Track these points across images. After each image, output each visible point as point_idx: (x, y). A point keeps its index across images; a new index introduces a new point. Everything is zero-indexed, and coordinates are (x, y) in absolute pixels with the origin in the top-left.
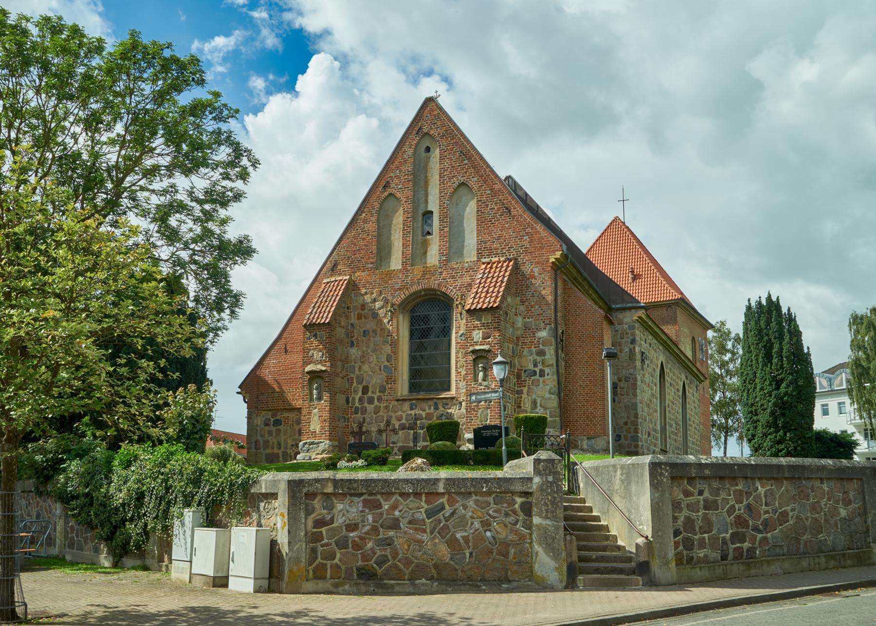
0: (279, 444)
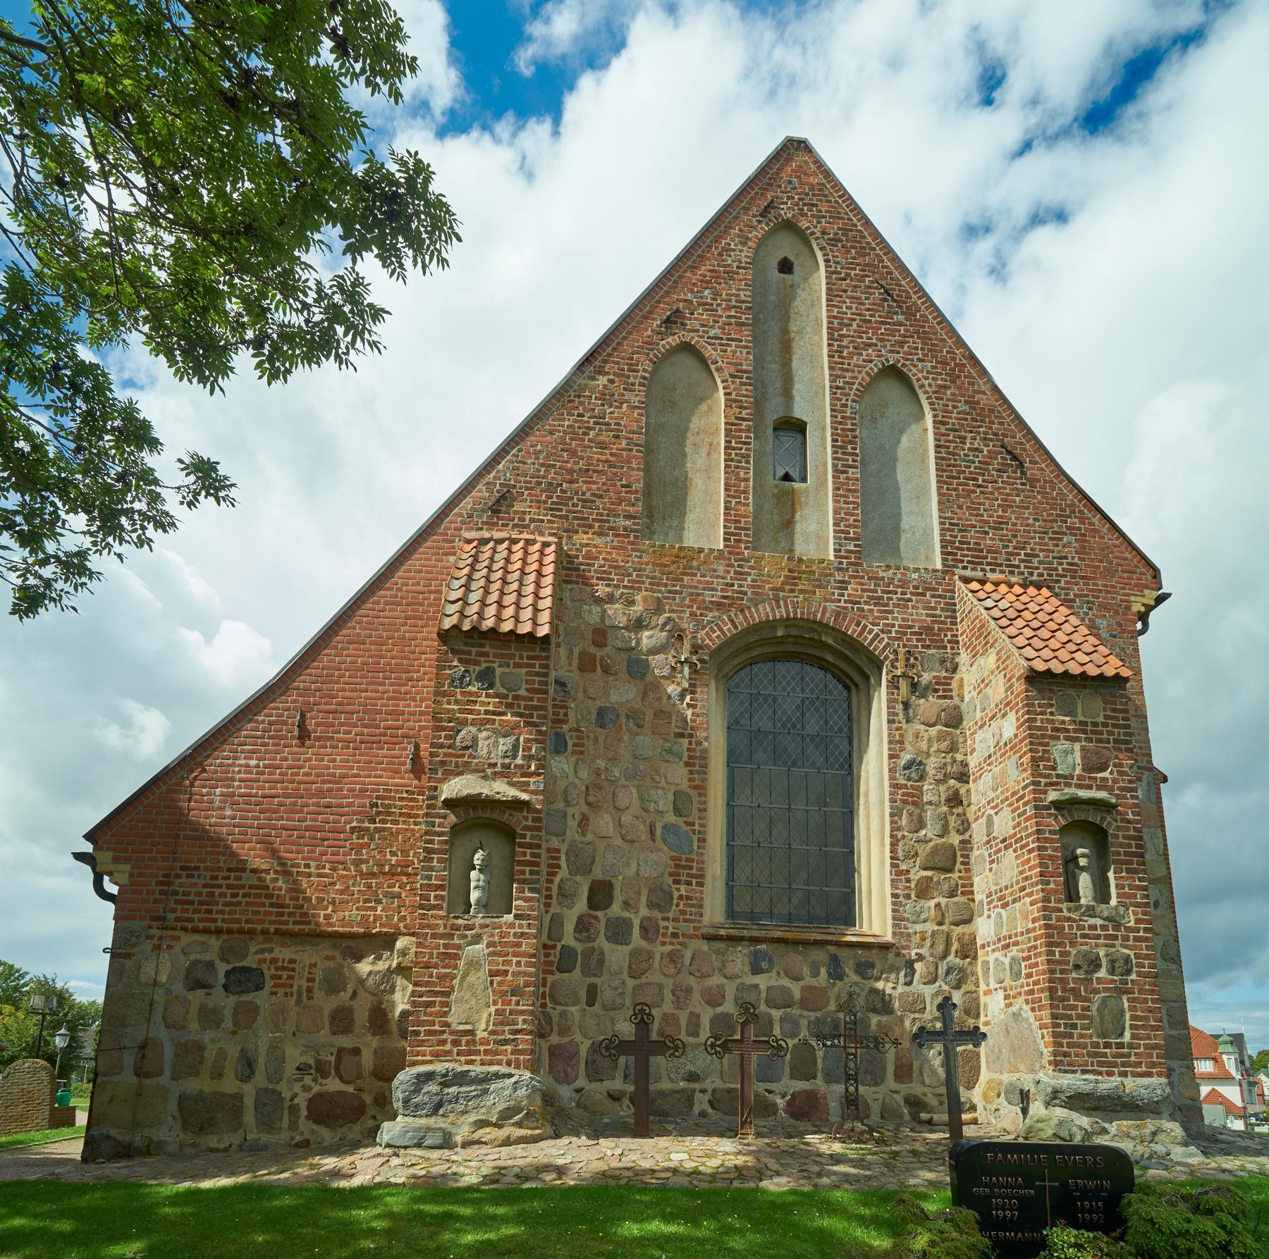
0: (248, 1065)
